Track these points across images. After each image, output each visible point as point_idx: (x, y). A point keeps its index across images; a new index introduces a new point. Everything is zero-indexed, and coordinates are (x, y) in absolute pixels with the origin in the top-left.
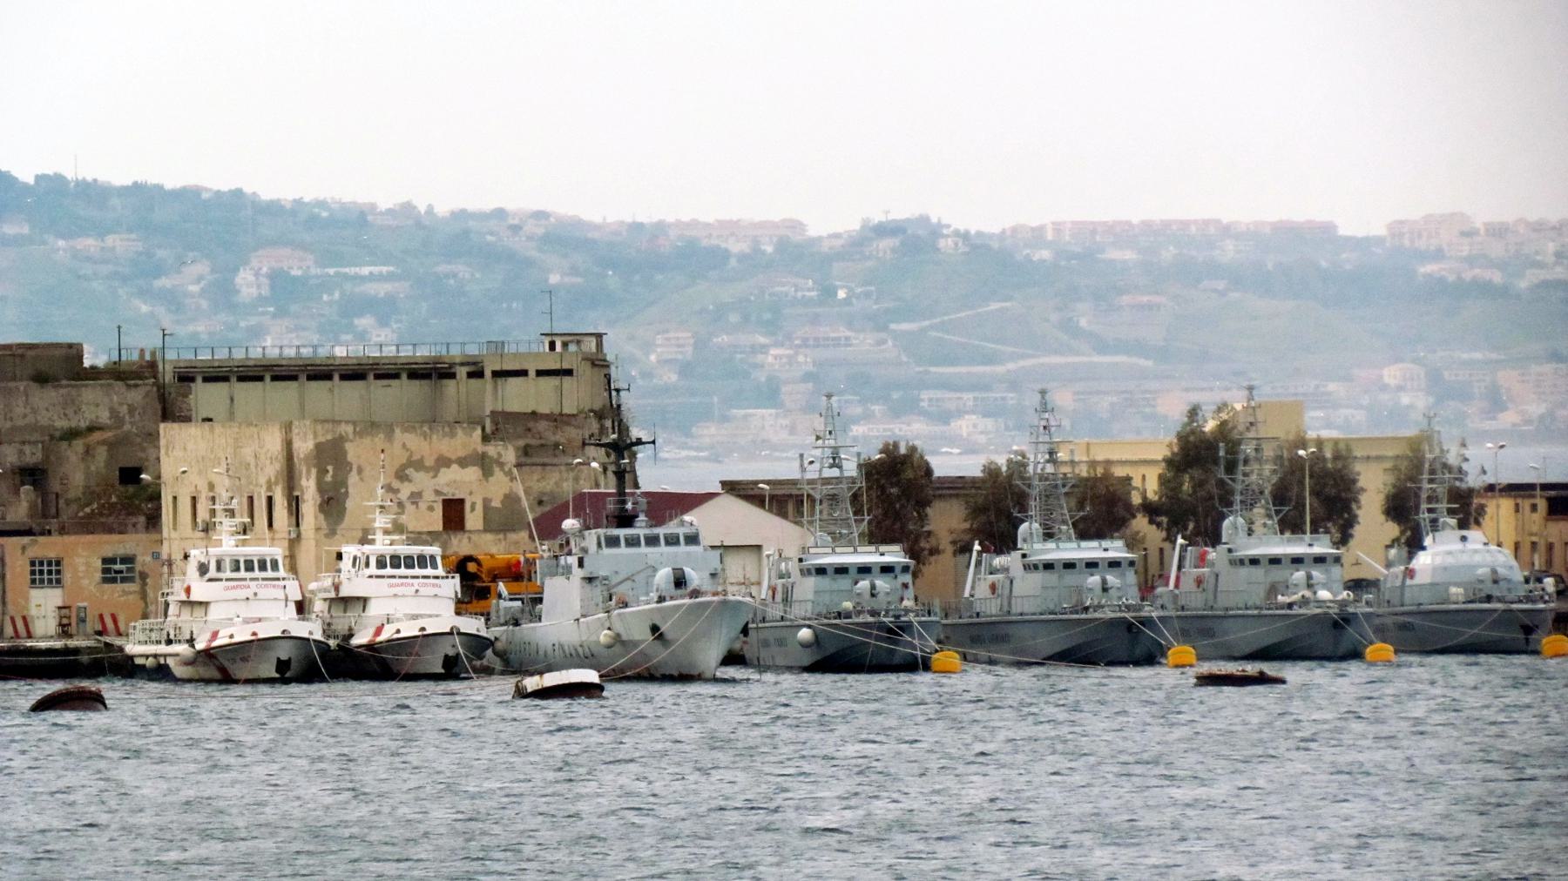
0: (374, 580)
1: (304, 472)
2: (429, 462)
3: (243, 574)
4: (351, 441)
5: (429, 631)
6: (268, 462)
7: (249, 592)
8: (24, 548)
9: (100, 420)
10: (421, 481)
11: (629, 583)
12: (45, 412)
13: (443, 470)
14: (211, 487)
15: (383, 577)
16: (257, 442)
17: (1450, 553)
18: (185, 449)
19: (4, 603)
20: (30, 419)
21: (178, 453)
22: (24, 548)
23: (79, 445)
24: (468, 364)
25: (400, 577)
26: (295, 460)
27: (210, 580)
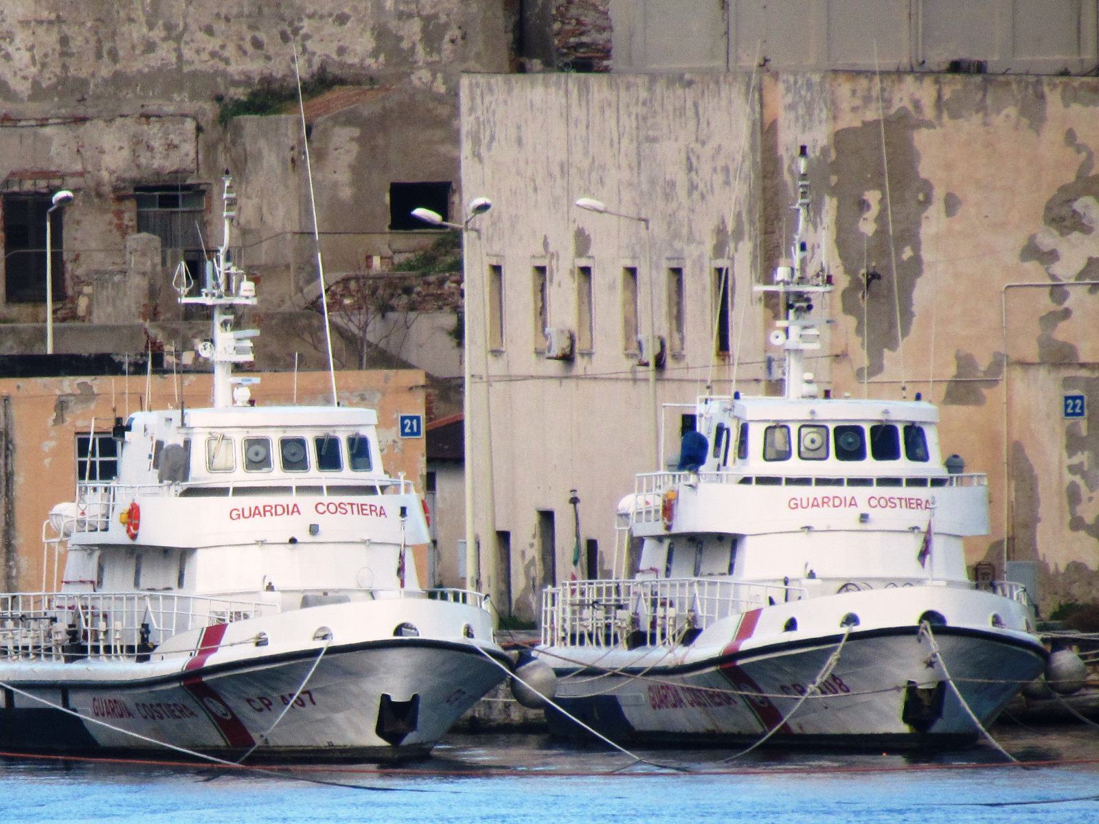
0: (754, 488)
4: (930, 125)
6: (719, 178)
7: (296, 526)
8: (61, 406)
9: (351, 59)
12: (201, 36)
14: (583, 241)
15: (775, 481)
16: (692, 125)
18: (519, 141)
19: (9, 547)
20: (165, 53)
21: (502, 151)
22: (61, 406)
23: (289, 125)
25: (822, 482)
27: (190, 492)
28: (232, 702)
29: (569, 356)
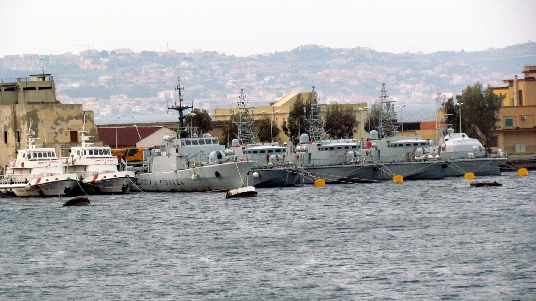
1: (22, 122)
2: (65, 118)
3: (43, 158)
5: (118, 177)
7: (47, 164)
10: (63, 125)
11: (194, 157)
13: (70, 121)
17: (460, 141)
24: (5, 86)
25: (99, 158)
26: (18, 118)
28: (42, 189)
29: (225, 133)
